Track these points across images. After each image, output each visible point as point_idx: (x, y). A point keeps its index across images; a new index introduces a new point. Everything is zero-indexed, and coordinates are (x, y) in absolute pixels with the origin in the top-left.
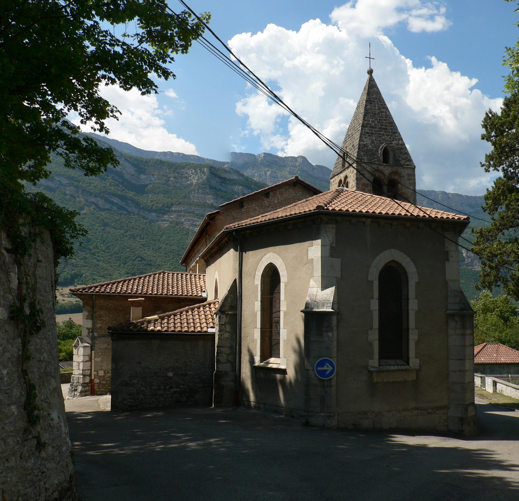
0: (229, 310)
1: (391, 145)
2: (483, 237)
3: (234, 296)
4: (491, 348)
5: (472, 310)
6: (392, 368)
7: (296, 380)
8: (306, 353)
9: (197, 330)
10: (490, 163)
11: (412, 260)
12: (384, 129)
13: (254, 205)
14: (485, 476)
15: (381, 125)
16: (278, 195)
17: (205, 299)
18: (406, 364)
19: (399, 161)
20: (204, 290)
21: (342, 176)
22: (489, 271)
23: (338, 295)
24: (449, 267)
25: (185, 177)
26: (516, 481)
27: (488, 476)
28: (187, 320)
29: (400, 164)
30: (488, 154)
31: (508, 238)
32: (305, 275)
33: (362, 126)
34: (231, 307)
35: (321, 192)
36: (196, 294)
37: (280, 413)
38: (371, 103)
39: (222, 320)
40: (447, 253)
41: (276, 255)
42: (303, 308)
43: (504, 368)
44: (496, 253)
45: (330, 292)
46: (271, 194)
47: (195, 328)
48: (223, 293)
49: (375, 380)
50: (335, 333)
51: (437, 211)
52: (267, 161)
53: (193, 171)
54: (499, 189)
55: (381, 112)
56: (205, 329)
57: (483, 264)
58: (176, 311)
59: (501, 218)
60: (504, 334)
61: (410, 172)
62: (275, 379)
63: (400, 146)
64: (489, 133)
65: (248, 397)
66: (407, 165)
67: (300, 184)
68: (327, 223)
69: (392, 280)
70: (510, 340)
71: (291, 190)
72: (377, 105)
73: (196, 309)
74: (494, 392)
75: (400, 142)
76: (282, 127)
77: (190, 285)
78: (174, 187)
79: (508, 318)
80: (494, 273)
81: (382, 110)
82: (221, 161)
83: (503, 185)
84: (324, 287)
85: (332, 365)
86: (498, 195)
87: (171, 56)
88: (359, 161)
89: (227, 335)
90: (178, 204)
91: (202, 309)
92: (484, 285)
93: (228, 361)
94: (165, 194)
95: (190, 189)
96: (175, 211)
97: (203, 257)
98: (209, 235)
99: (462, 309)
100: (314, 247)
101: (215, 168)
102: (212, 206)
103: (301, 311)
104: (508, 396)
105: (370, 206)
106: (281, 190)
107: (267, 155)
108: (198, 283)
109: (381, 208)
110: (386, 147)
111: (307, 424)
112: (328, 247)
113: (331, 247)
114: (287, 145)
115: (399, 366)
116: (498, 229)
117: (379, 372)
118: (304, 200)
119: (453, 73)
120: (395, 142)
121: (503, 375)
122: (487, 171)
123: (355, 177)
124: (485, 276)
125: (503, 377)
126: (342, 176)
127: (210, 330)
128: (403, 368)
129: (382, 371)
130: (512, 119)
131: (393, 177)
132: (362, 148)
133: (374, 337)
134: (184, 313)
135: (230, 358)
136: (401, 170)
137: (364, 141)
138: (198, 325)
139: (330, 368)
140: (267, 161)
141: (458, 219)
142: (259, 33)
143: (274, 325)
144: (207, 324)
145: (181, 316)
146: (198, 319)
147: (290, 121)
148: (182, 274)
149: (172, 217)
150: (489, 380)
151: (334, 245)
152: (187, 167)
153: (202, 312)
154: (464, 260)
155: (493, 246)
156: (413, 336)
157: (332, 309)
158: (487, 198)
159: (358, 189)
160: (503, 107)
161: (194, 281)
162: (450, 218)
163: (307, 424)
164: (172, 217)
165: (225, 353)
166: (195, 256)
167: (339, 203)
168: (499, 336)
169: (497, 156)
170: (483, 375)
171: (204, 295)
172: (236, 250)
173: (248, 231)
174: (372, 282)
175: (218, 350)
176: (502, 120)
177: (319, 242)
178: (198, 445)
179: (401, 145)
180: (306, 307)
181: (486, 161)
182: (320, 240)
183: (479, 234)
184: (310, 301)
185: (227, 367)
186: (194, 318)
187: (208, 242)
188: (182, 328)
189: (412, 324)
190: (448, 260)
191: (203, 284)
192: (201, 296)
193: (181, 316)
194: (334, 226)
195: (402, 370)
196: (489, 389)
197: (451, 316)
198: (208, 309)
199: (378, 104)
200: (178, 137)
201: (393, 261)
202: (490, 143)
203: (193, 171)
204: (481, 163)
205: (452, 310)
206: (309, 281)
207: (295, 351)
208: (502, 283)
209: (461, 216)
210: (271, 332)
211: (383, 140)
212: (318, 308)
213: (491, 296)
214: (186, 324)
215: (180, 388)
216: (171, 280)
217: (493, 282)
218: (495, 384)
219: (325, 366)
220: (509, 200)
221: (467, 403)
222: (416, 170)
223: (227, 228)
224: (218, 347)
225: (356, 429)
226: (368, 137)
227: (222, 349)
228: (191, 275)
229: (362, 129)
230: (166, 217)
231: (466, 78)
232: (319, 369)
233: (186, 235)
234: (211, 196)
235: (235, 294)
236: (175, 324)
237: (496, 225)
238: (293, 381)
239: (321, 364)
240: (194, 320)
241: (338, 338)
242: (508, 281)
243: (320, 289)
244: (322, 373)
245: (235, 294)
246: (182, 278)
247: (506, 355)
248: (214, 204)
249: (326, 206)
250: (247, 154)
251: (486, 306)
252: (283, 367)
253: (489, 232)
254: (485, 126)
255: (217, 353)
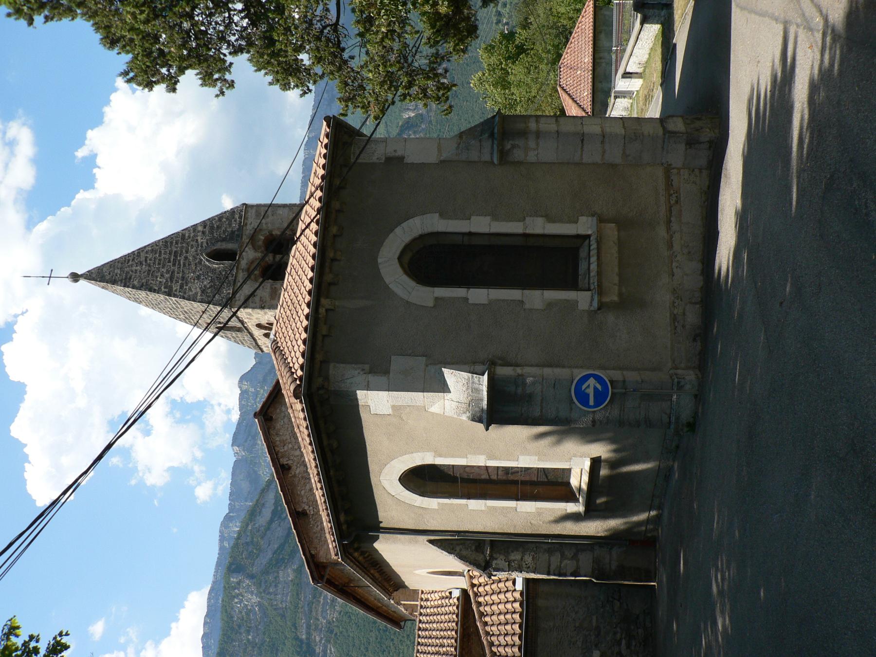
0: (483, 553)
1: (205, 244)
2: (354, 96)
3: (458, 545)
4: (566, 78)
5: (494, 117)
6: (594, 267)
7: (612, 441)
8: (563, 424)
9: (519, 609)
10: (217, 80)
11: (399, 223)
12: (176, 256)
13: (303, 492)
14: (806, 117)
15: (169, 262)
16: (286, 448)
17: (464, 592)
18: (587, 241)
19: (233, 232)
20: (448, 594)
21: (258, 333)
22: (416, 88)
23: (457, 364)
24: (413, 156)
25: (247, 614)
26: (818, 57)
27: (806, 112)
28: (500, 624)
29: (238, 230)
30: (200, 82)
31: (357, 49)
32: (419, 421)
33: (169, 295)
34: (481, 550)
35: (278, 382)
36: (455, 608)
37: (670, 469)
38: (130, 278)
39: (501, 566)
40: (389, 160)
41: (386, 470)
42: (481, 427)
43: (601, 58)
44: (384, 74)
45: (451, 376)
46: (284, 461)
47: (514, 612)
48: (453, 563)
49: (616, 298)
50: (528, 370)
51: (313, 175)
52: (246, 441)
53: (236, 600)
54: (269, 63)
55: (146, 260)
56: (517, 595)
57: (405, 98)
58: (485, 643)
59: (319, 62)
60: (544, 55)
61: (252, 213)
62: (609, 478)
63: (207, 230)
64: (163, 79)
65: (639, 524)
66: (240, 217)
67: (268, 409)
68: (327, 378)
69: (433, 261)
70: (553, 46)
71: (278, 426)
72: (134, 268)
73: (482, 609)
74: (641, 77)
75: (200, 228)
76: (190, 413)
77: (439, 617)
78: (264, 634)
79: (517, 47)
80: (420, 81)
81: (143, 259)
82: (217, 552)
83: (262, 55)
84: (443, 388)
85: (586, 378)
86: (279, 64)
87: (27, 639)
88: (226, 304)
89: (528, 559)
90: (296, 628)
91: (481, 599)
92: (443, 98)
93: (575, 557)
94: (277, 650)
95: (269, 608)
96: (309, 634)
97: (389, 594)
98: (351, 581)
99: (492, 135)
100: (370, 403)
101: (231, 564)
102: (299, 571)
103: (487, 429)
104: (650, 54)
105: (300, 297)
106: (278, 443)
107: (235, 441)
108: (436, 603)
109: (304, 278)
110: (208, 255)
111: (692, 426)
112: (370, 377)
113: (370, 373)
114: (220, 404)
115: (592, 253)
116: (340, 69)
117: (601, 292)
118: (290, 411)
119: (106, 119)
120: (199, 238)
121: (614, 60)
122: (232, 84)
123: (259, 311)
124: (425, 96)
125: (617, 61)
126: (258, 333)
127: (519, 586)
128: (594, 246)
129: (600, 286)
130: (138, 35)
131: (260, 243)
132: (209, 296)
133: (537, 298)
134: (488, 629)
135: (569, 553)
136: (249, 230)
137: (196, 294)
138: (509, 606)
139: (592, 382)
140: (246, 441)
141: (327, 137)
142: (26, 450)
143: (511, 477)
144: (507, 591)
145: (493, 635)
146: (500, 606)
147: (181, 398)
148: (420, 629)
149: (318, 639)
150: (621, 84)
151: (367, 367)
152: (229, 610)
153: (487, 598)
154: (421, 115)
155: (371, 80)
156: (538, 226)
157: (483, 374)
158: (285, 85)
159: (274, 307)
160: (116, 50)
161: (432, 610)
162: (325, 151)
163: (692, 426)
164: (318, 639)
165: (561, 562)
166: (387, 606)
167: (293, 354)
168: (547, 64)
169: (205, 65)
170: (613, 95)
171: (456, 594)
172: (376, 538)
173: (342, 518)
174: (437, 299)
175: (555, 575)
176: (138, 54)
177: (361, 394)
178: (723, 612)
179: (205, 227)
180: (480, 421)
181: (215, 86)
182: (358, 392)
183: (350, 104)
184: (468, 414)
185: (586, 560)
186: (498, 612)
187: (362, 584)
188: (514, 634)
189: (514, 228)
190: (402, 158)
191: (436, 595)
192: (458, 599)
193: (493, 635)
194: (332, 365)
195: (599, 249)
196: (635, 85)
197: (504, 156)
198: (481, 589)
199: (132, 265)
200: (177, 620)
201: (400, 259)
202: (181, 78)
203: (236, 600)
204: (217, 96)
205: (492, 154)
206: (433, 414)
207: (559, 442)
208: (440, 65)
209: (323, 132)
210: (524, 483)
211: (195, 258)
212: (482, 400)
213: (480, 73)
214: (508, 627)
215: (621, 639)
216: (429, 648)
217: (439, 81)
218: (627, 75)
219: (587, 391)
220: (286, 46)
221: (660, 132)
222: (250, 202)
223: (336, 555)
224: (548, 574)
225: (703, 335)
226: (190, 285)
227: (553, 567)
228: (421, 614)
229: (175, 296)
230: (318, 650)
231: (113, 97)
232: (591, 403)
233: (350, 617)
234: (281, 573)
235: (455, 542)
236: (507, 645)
237: (332, 73)
238: (613, 447)
239: (583, 398)
240: (500, 614)
241: (537, 366)
242: (437, 53)
243: (448, 396)
244: (600, 396)
245: (455, 542)
246: (426, 630)
247: (579, 52)
248: (295, 567)
249: (296, 379)
250: (233, 474)
251: (497, 83)
252: (587, 464)
253: (346, 84)
254: (149, 85)
255: (560, 576)
